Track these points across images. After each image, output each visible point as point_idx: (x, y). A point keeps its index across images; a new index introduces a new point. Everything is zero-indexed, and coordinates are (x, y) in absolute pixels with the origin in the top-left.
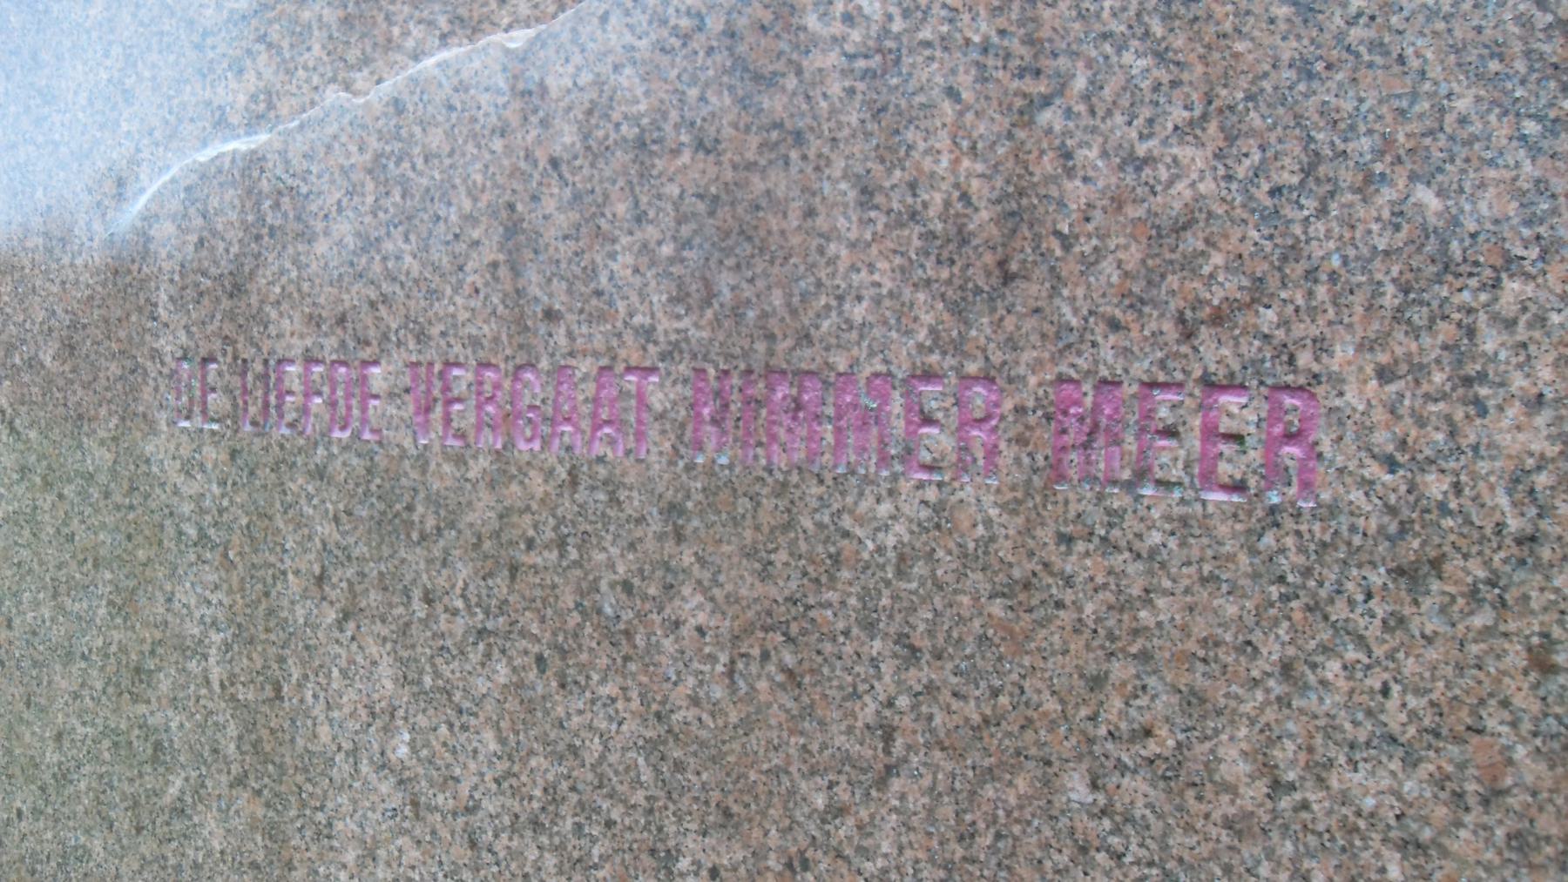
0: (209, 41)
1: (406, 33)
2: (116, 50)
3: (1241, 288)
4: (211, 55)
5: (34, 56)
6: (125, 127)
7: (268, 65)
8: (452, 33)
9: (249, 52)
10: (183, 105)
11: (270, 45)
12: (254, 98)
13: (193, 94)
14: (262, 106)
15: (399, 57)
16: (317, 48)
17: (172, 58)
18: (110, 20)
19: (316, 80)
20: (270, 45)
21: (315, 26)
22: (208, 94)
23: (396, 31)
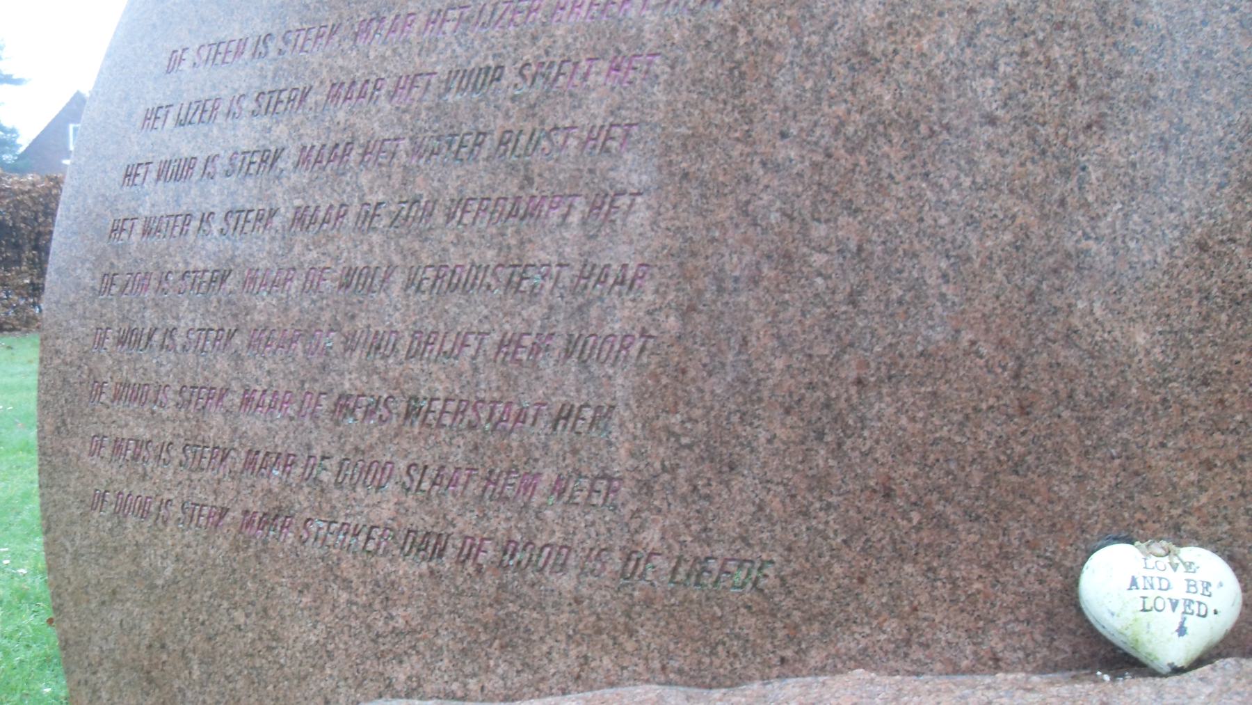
0: (381, 640)
1: (497, 666)
2: (320, 627)
3: (1188, 523)
4: (382, 648)
5: (265, 610)
6: (328, 671)
7: (417, 663)
8: (522, 671)
9: (406, 653)
10: (366, 671)
11: (418, 652)
12: (410, 678)
13: (371, 665)
14: (415, 684)
15: (493, 677)
16: (446, 661)
17: (358, 642)
18: (317, 608)
19: (446, 678)
20: (418, 652)
21: (445, 648)
22: (381, 668)
23: (492, 663)
